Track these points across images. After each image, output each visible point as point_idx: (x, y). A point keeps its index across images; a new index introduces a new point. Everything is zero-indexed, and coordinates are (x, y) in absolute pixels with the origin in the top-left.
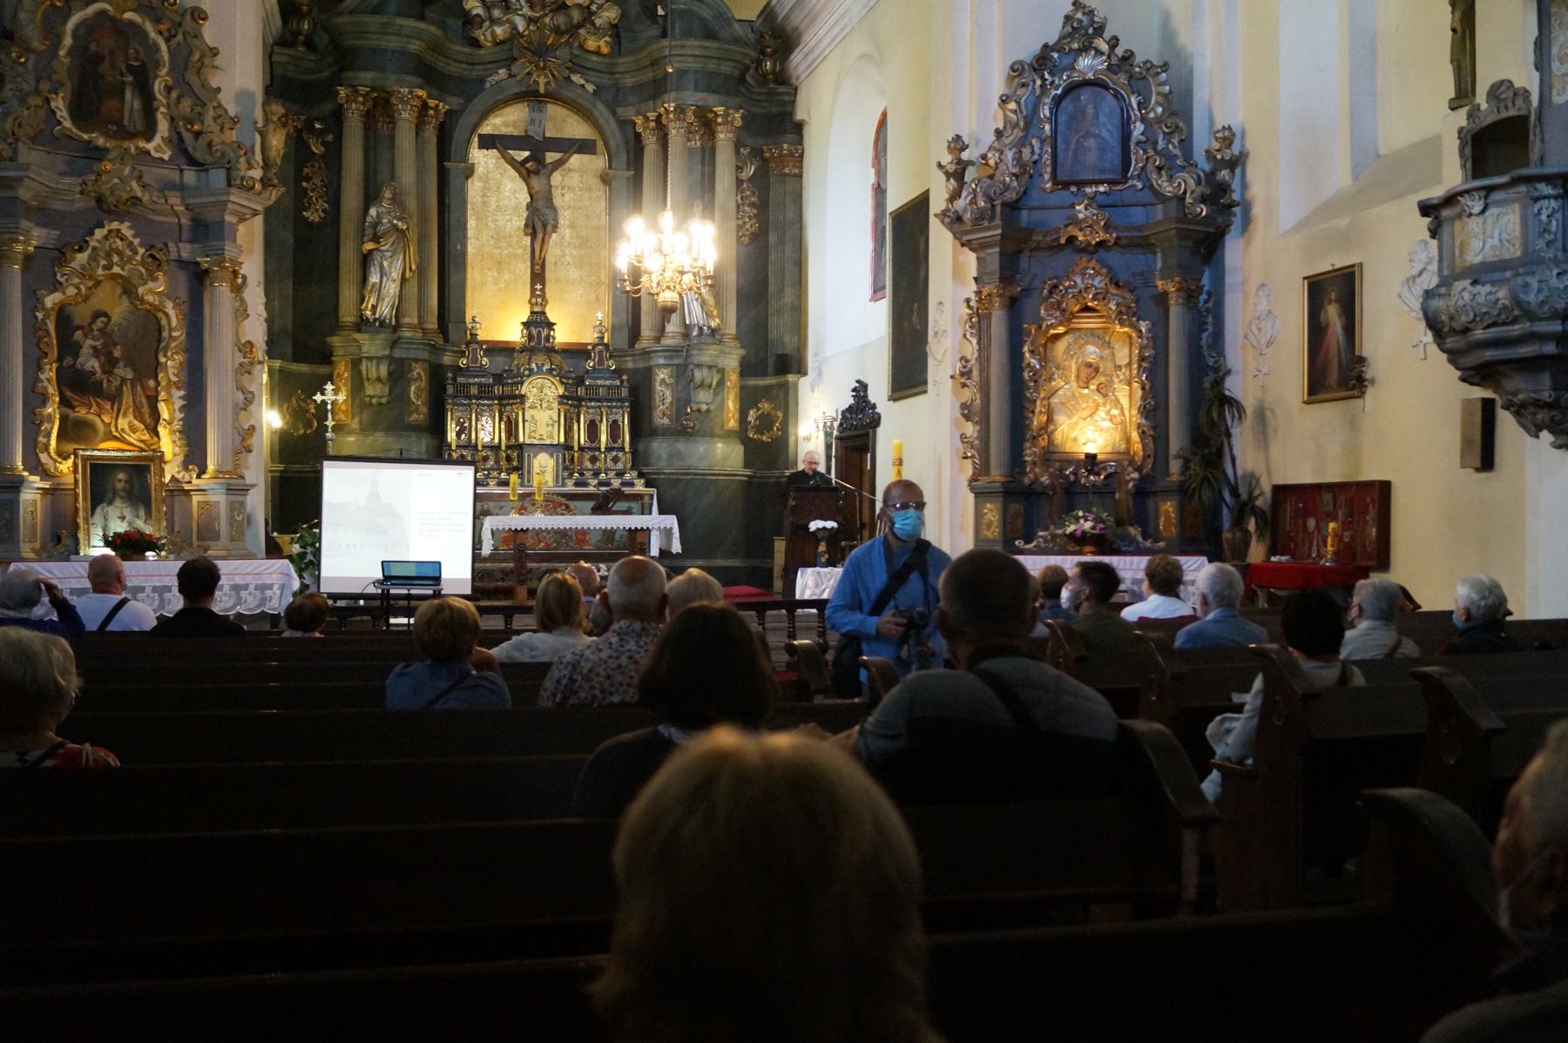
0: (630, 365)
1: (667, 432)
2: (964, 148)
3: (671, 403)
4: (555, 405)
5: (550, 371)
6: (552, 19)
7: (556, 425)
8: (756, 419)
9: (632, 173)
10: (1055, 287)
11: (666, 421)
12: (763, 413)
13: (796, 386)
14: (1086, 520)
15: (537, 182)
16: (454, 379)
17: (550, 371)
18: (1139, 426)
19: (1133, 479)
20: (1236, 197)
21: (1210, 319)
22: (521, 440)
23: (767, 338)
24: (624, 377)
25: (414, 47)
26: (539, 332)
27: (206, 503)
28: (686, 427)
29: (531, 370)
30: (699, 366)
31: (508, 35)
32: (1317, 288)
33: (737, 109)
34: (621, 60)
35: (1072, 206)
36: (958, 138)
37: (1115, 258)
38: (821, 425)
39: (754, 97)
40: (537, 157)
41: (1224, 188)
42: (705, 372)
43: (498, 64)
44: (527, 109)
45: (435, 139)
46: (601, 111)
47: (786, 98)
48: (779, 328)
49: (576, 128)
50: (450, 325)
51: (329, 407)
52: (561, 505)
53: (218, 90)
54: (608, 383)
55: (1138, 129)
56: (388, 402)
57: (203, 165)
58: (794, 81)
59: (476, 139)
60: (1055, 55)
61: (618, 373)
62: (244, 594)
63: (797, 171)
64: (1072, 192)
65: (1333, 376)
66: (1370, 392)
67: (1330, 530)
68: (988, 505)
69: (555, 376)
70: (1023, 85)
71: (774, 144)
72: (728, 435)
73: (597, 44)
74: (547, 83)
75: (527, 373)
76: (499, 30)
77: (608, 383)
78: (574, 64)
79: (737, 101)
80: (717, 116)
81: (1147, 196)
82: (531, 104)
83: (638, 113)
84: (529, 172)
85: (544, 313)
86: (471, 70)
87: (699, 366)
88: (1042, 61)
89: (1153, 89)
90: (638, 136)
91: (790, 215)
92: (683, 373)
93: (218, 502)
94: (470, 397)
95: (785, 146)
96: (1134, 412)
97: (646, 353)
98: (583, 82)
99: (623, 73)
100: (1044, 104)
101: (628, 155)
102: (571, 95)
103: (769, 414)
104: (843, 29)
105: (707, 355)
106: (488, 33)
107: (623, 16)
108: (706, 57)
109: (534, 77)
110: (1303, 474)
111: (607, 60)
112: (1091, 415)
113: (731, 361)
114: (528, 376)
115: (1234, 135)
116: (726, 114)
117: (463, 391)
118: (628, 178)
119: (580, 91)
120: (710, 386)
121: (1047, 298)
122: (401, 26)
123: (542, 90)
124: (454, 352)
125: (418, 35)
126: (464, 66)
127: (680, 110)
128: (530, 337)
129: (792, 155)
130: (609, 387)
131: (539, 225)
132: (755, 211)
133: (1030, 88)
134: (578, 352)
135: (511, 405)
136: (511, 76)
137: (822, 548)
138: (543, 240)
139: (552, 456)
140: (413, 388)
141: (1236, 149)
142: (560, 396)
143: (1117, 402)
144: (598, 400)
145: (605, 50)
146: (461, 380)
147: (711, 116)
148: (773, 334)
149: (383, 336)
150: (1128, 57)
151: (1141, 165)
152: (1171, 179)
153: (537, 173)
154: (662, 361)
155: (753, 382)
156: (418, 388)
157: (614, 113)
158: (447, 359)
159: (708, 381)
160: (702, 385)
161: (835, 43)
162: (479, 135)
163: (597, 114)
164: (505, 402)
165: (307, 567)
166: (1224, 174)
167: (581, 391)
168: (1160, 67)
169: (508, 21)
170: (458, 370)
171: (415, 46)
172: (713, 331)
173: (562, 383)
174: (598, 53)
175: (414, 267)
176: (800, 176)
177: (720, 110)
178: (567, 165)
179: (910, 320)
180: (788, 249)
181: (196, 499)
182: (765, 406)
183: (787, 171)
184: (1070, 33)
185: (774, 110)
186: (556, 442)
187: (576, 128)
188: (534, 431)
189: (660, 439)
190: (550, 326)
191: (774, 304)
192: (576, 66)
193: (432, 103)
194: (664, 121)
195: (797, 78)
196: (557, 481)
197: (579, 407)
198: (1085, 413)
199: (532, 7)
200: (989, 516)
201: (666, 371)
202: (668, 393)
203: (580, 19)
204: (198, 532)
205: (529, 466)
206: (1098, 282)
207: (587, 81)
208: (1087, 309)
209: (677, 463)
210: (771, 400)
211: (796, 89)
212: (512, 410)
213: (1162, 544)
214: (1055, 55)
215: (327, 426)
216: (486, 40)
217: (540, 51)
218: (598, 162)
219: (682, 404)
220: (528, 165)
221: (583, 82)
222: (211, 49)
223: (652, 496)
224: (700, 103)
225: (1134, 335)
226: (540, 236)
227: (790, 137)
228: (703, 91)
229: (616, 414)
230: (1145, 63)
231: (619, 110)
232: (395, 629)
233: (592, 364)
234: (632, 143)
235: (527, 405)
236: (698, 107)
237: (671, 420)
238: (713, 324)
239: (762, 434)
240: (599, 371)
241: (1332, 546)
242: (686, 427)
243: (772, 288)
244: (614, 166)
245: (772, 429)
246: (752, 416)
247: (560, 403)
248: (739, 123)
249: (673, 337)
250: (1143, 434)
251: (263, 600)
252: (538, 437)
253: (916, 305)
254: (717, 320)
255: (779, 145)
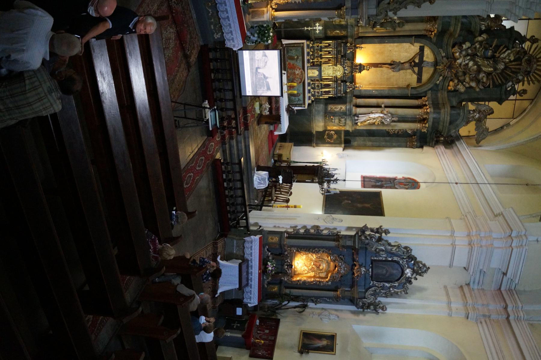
0: (348, 96)
1: (326, 109)
2: (386, 234)
3: (335, 111)
4: (334, 75)
5: (345, 73)
6: (460, 71)
7: (328, 75)
8: (331, 134)
9: (410, 95)
10: (342, 260)
11: (329, 109)
12: (333, 136)
13: (341, 147)
14: (272, 267)
15: (407, 65)
16: (343, 42)
17: (345, 73)
18: (301, 280)
19: (284, 279)
20: (366, 310)
21: (331, 301)
22: (323, 65)
23: (357, 136)
24: (344, 95)
25: (451, 29)
26: (357, 69)
27: (264, 13)
28: (328, 114)
29: (345, 67)
30: (346, 120)
31: (456, 57)
32: (332, 338)
33: (427, 131)
34: (446, 93)
35: (365, 267)
36: (389, 233)
37: (350, 276)
38: (324, 161)
39: (432, 134)
40: (416, 65)
41: (368, 307)
42: (344, 122)
43: (446, 52)
44: (432, 61)
45: (422, 34)
46: (430, 86)
47: (431, 144)
48: (359, 141)
49: (425, 77)
50: (361, 39)
51: (314, 28)
52: (301, 80)
53: (406, 8)
54: (342, 90)
55: (388, 285)
56: (333, 24)
57: (378, 7)
58: (437, 146)
59: (423, 45)
60: (413, 262)
61: (346, 93)
62: (230, 34)
63: (408, 146)
64: (370, 265)
65: (307, 342)
66: (298, 354)
67: (261, 341)
68: (278, 239)
69: (343, 75)
70: (404, 253)
71: (417, 140)
72: (325, 126)
73: (451, 85)
74: (440, 69)
75: (344, 66)
76: (458, 54)
77: (342, 90)
78: (446, 78)
79: (430, 130)
80: (426, 124)
81: (367, 287)
82: (434, 62)
83: (428, 98)
84: (411, 63)
85: (364, 69)
86: (445, 44)
87: (346, 120)
88: (412, 258)
89: (399, 290)
90: (421, 98)
91: (394, 144)
92: (344, 114)
93: (264, 17)
94: (337, 48)
95: (416, 143)
96: (305, 278)
97: (351, 101)
98: (440, 80)
99: (442, 93)
100: (397, 259)
101: (416, 94)
102: (436, 76)
103: (333, 138)
104: (447, 171)
105: (349, 122)
106: (456, 51)
107: (461, 93)
108: (444, 122)
109: (442, 65)
110: (282, 329)
111: (446, 88)
112: (305, 265)
113: (349, 127)
114: (343, 67)
115: (385, 311)
116: (425, 127)
117: (337, 46)
118: (408, 94)
119: (437, 79)
120: (339, 123)
121: (339, 256)
122: (458, 25)
123: (438, 67)
124: (352, 42)
125: (455, 30)
126: (446, 43)
127: (427, 113)
128: (357, 66)
129: (413, 145)
130: (341, 90)
131: (393, 66)
132: (396, 133)
133: (403, 255)
134: (353, 80)
135: (334, 61)
136: (443, 57)
137: (274, 179)
138: (388, 68)
139: (317, 75)
140: (338, 31)
141: (380, 311)
142: (337, 77)
143: (308, 272)
144: (336, 87)
145: (449, 88)
146: (343, 45)
147: (426, 122)
148: (357, 138)
149: (354, 23)
150: (410, 282)
151: (377, 285)
152: (372, 295)
153: (410, 66)
154: (348, 107)
155: (343, 133)
156: (338, 33)
157: (430, 89)
158: (350, 39)
159: (341, 122)
160: (340, 120)
161: (443, 166)
162: (424, 46)
163: (429, 84)
164: (335, 58)
165: (260, 28)
166: (372, 307)
167: (339, 82)
168: (406, 292)
169: (461, 57)
170: (347, 43)
171: (452, 29)
172: (356, 124)
173: (341, 77)
174: (448, 85)
175: (377, 31)
176: (406, 147)
177: (427, 125)
178: (414, 74)
179: (347, 199)
180: (384, 143)
181: (265, 9)
182: (335, 137)
183: (408, 143)
184: (419, 266)
185: (428, 140)
186: (323, 75)
187: (425, 77)
188: (326, 69)
189: (324, 107)
190: (360, 72)
191: (367, 138)
192: (445, 78)
193: (433, 33)
194: (425, 107)
195: (437, 148)
196: (310, 77)
197: (334, 82)
198: (306, 264)
199: (464, 65)
200: (275, 239)
201: (345, 109)
202: (338, 110)
203: (461, 80)
204: (255, 11)
205: (314, 69)
206: (342, 271)
207: (440, 81)
208: (336, 267)
209: (316, 113)
210: (337, 138)
211: (434, 147)
212: (333, 62)
213: (266, 286)
214: (413, 262)
215: (308, 27)
216: (454, 50)
217: (450, 67)
218: (414, 83)
219: (334, 114)
220: (413, 63)
221: (440, 80)
222: (420, 5)
223: (304, 107)
224: (429, 119)
225: (327, 280)
226: (390, 67)
227: (419, 144)
228: (433, 121)
229: (333, 92)
230: (408, 288)
231: (430, 91)
232: (203, 112)
233: (348, 84)
234: (419, 95)
235: (334, 67)
236: (428, 119)
237: (329, 111)
238: (359, 124)
239: (327, 135)
240: (346, 87)
241: (257, 341)
242: (328, 114)
243: (372, 138)
244: (412, 90)
245: (328, 139)
246: (333, 132)
247: (335, 76)
248: (423, 131)
249: (355, 111)
250: (298, 281)
251: (229, 40)
252: (324, 70)
253: (350, 202)
254: (360, 125)
255: (416, 141)
